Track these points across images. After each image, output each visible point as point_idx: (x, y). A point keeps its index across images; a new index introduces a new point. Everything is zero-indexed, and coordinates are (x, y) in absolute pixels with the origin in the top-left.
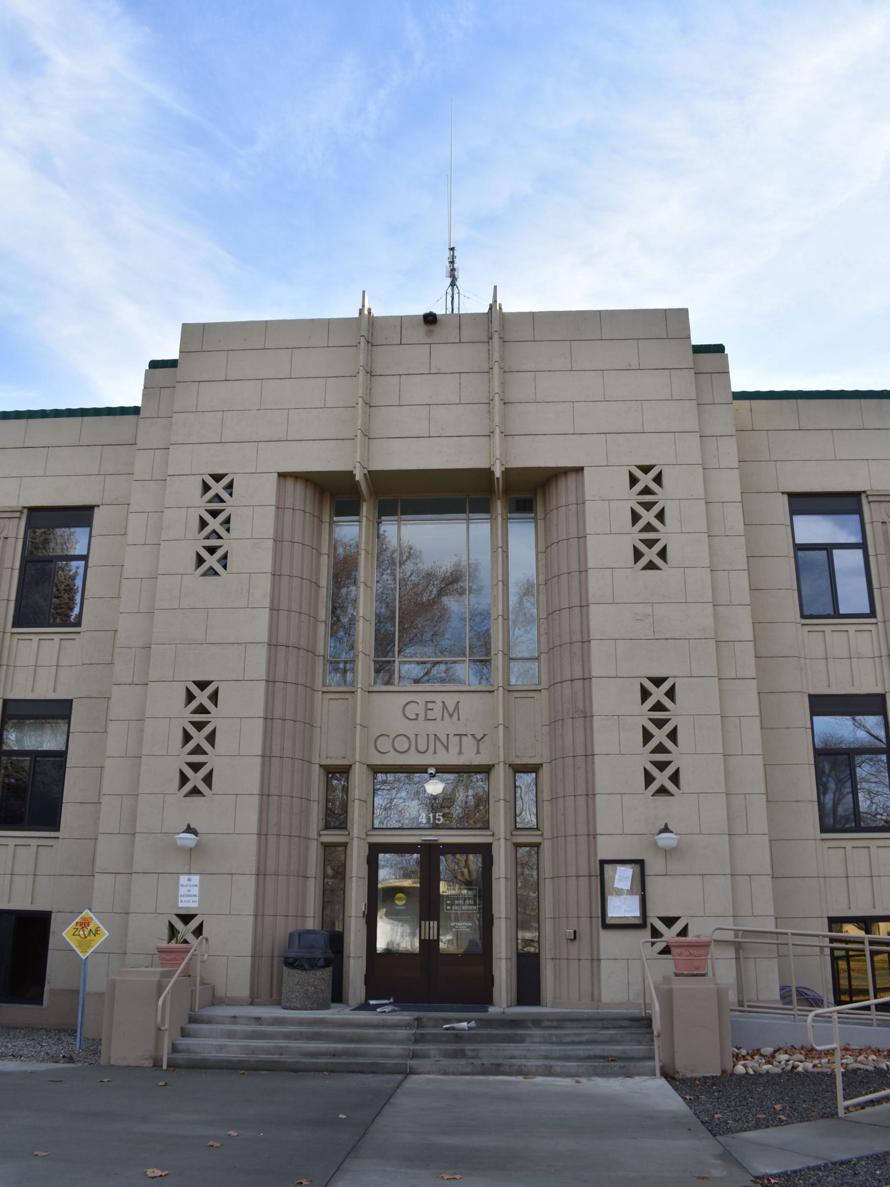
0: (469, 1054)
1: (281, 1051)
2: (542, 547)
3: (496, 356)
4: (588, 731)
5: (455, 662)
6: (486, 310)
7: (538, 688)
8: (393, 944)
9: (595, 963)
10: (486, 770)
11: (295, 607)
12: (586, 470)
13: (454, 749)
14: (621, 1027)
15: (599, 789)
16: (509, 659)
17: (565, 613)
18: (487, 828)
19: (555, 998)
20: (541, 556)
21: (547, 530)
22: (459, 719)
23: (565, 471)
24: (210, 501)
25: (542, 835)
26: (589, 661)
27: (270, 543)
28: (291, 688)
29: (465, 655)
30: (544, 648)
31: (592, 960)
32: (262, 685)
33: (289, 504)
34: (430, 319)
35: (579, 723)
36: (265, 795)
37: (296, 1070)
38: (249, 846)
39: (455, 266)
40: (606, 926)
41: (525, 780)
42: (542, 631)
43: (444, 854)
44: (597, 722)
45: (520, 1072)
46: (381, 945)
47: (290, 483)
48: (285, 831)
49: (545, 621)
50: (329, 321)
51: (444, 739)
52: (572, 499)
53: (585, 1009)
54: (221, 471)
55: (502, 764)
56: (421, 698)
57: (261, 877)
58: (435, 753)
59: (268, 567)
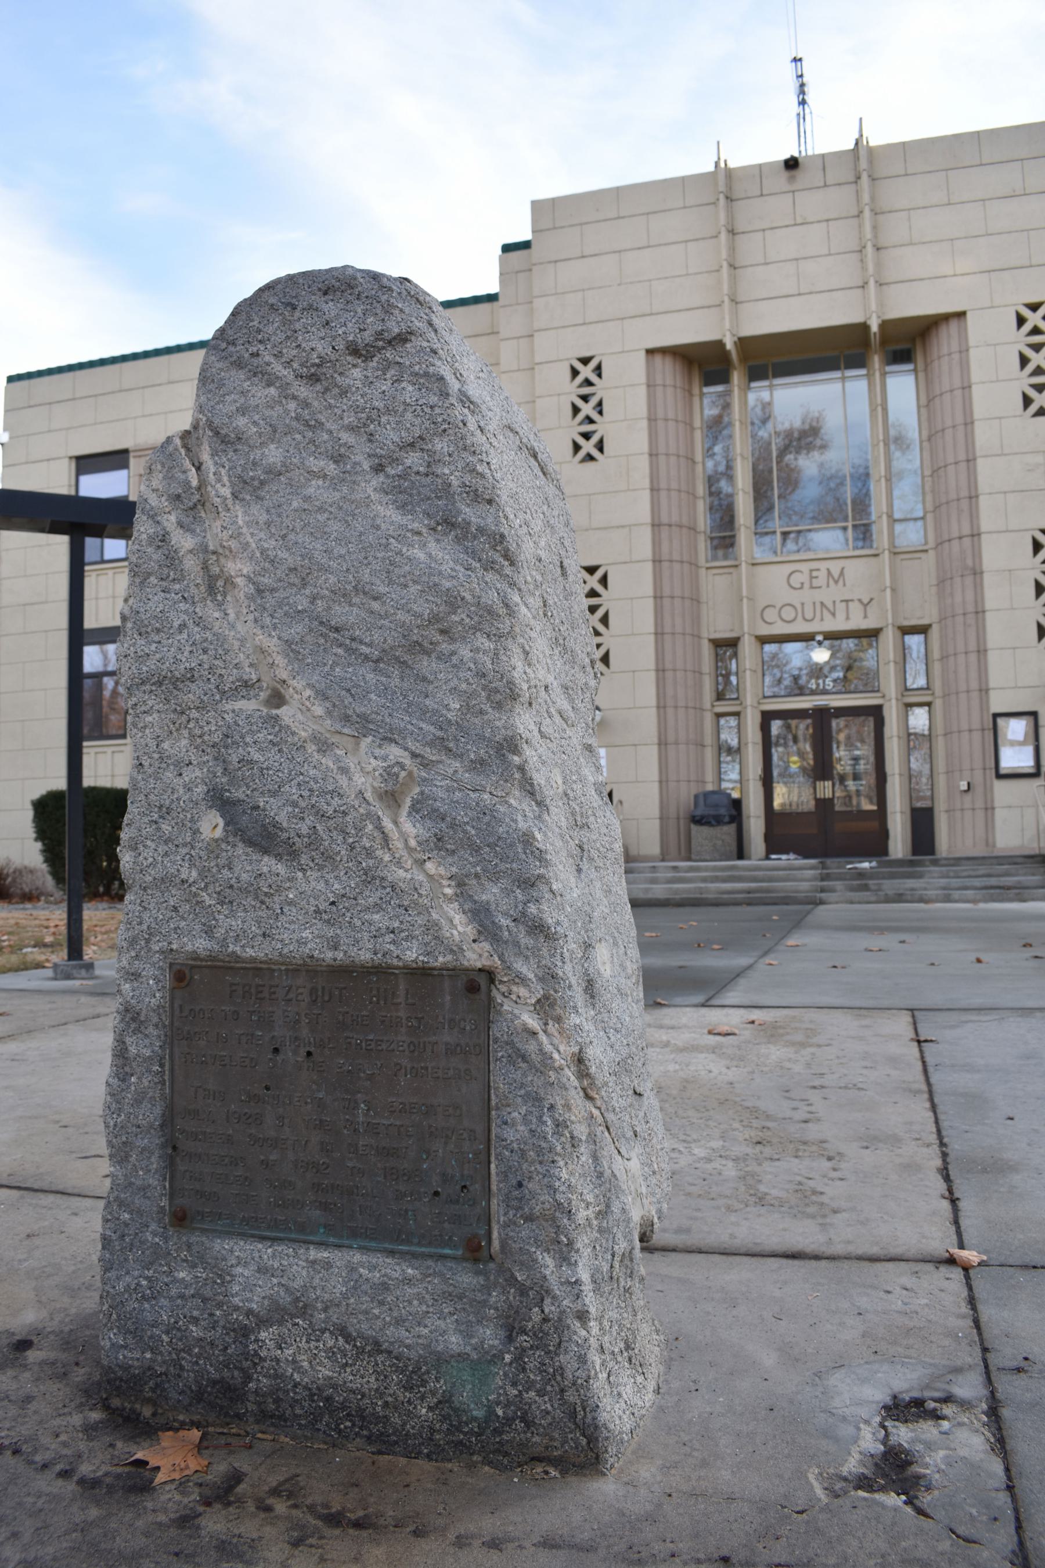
0: (873, 887)
1: (701, 890)
2: (923, 401)
3: (866, 198)
4: (978, 588)
5: (810, 530)
6: (851, 146)
7: (925, 548)
8: (791, 805)
9: (989, 812)
10: (873, 634)
11: (674, 485)
12: (969, 315)
13: (841, 615)
14: (1015, 864)
15: (990, 645)
16: (893, 521)
17: (951, 469)
18: (878, 691)
19: (950, 847)
20: (923, 411)
21: (928, 382)
22: (844, 585)
23: (945, 318)
24: (580, 386)
25: (933, 694)
26: (978, 517)
27: (644, 424)
28: (677, 566)
29: (846, 519)
30: (930, 506)
31: (985, 769)
32: (649, 566)
33: (659, 381)
34: (792, 164)
35: (969, 580)
36: (660, 671)
37: (716, 904)
38: (649, 718)
39: (805, 79)
40: (999, 776)
41: (915, 642)
42: (927, 488)
43: (837, 717)
44: (987, 578)
45: (921, 900)
46: (777, 803)
47: (658, 359)
48: (681, 703)
49: (930, 479)
50: (683, 179)
51: (830, 606)
52: (955, 346)
53: (980, 851)
54: (587, 354)
55: (890, 627)
56: (805, 567)
57: (663, 747)
58: (822, 620)
59: (645, 447)
